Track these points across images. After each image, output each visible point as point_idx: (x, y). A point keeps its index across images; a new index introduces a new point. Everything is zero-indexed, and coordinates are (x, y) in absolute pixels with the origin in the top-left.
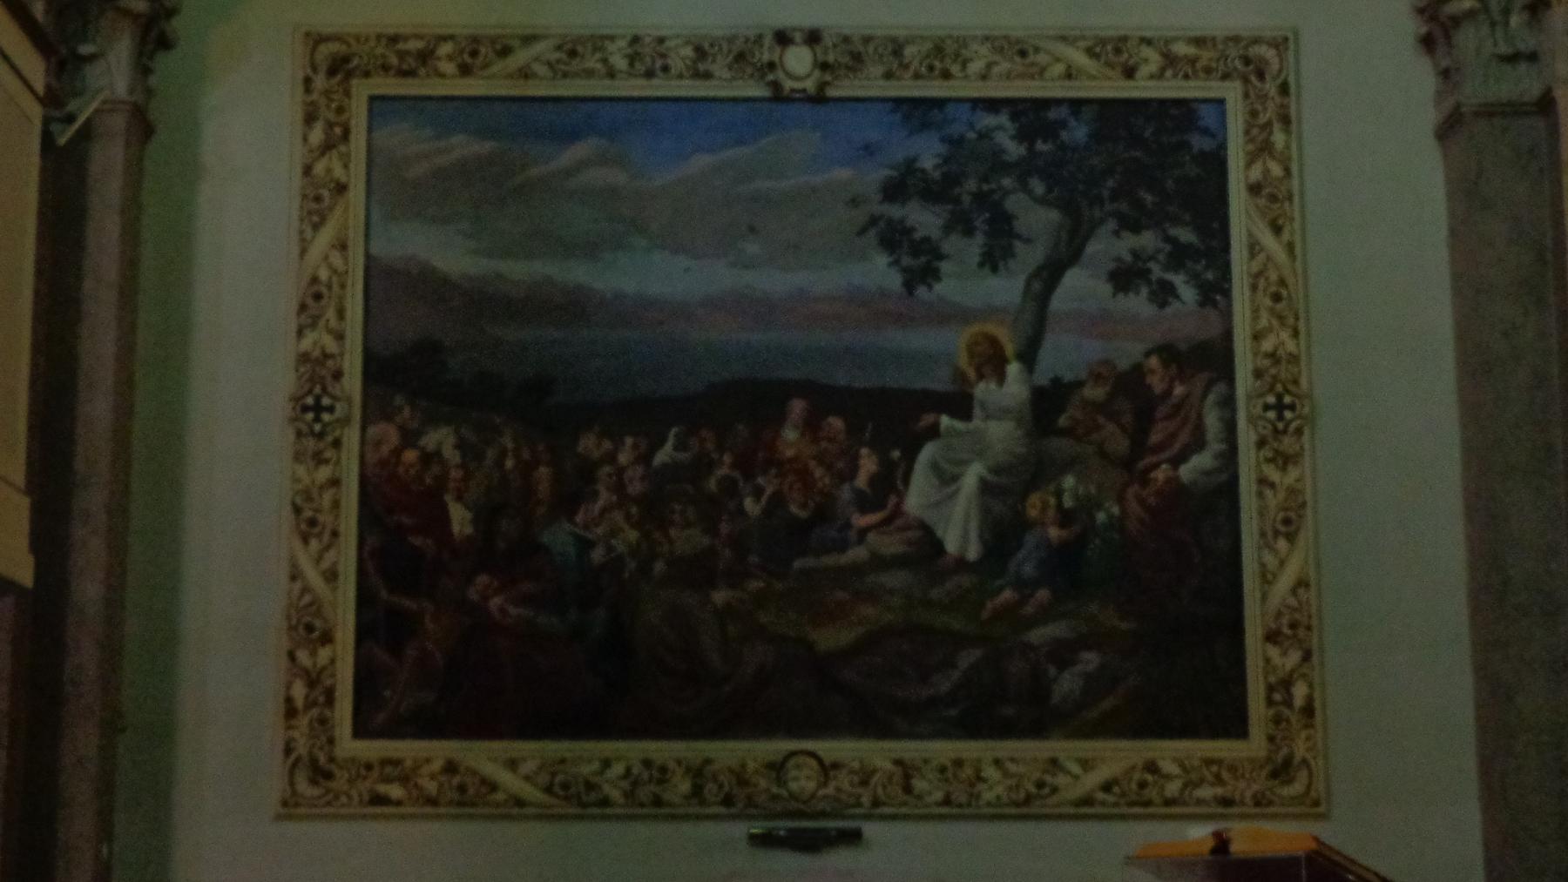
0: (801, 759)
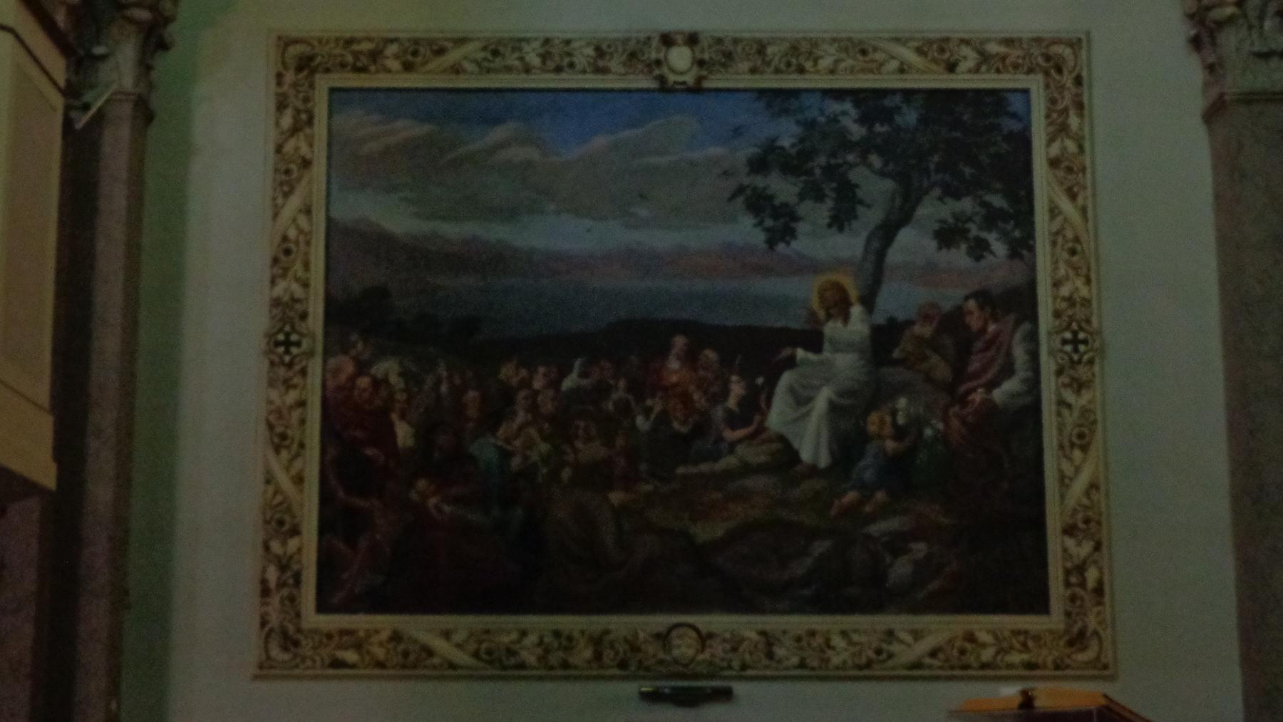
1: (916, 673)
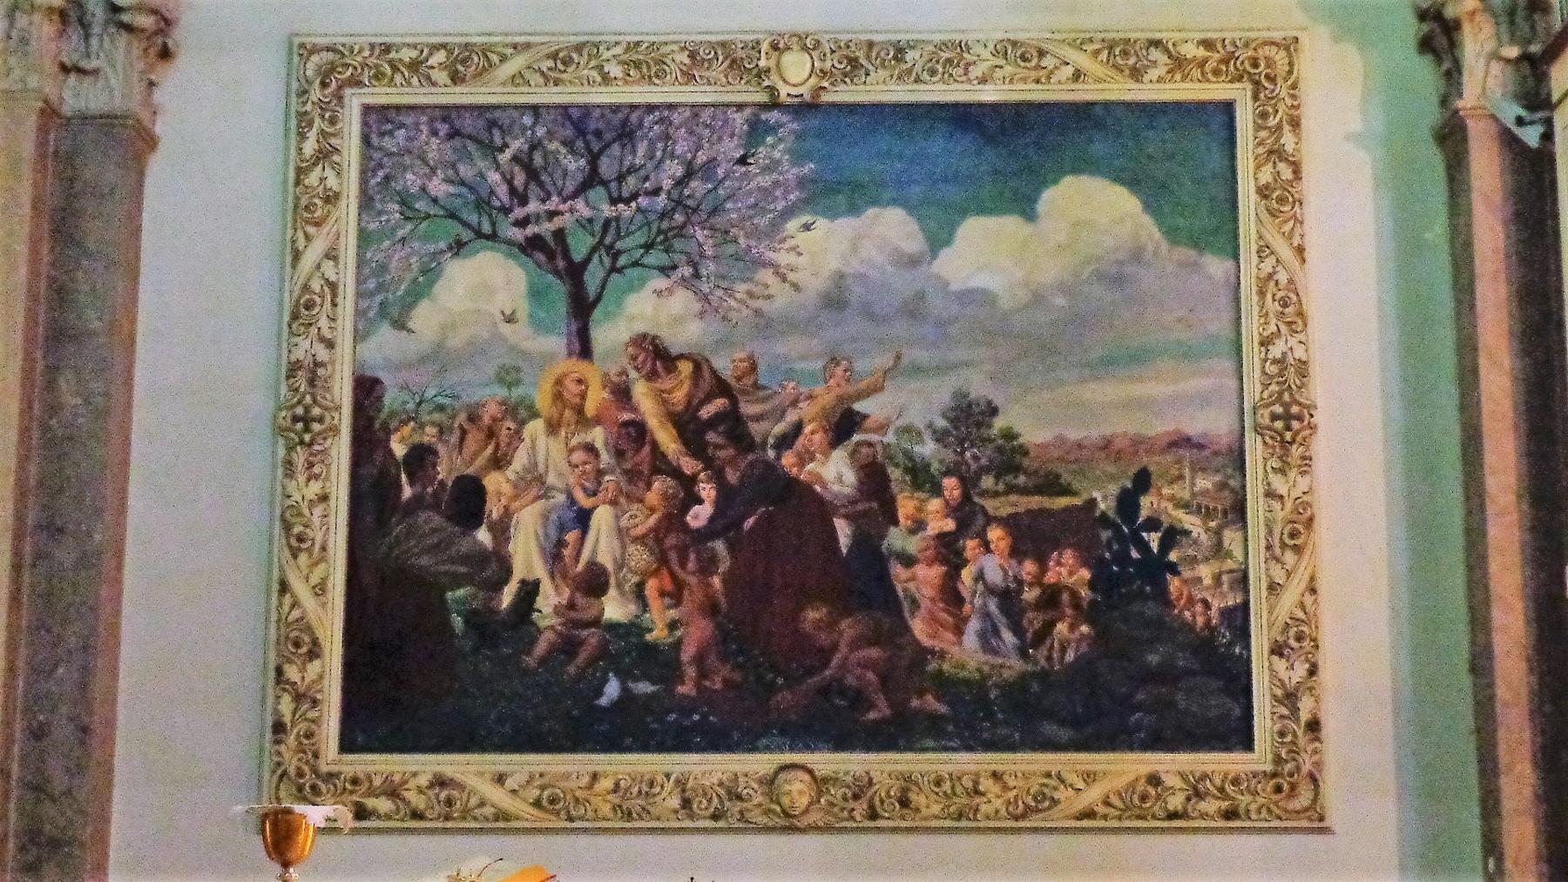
0: (791, 775)
1: (1086, 823)
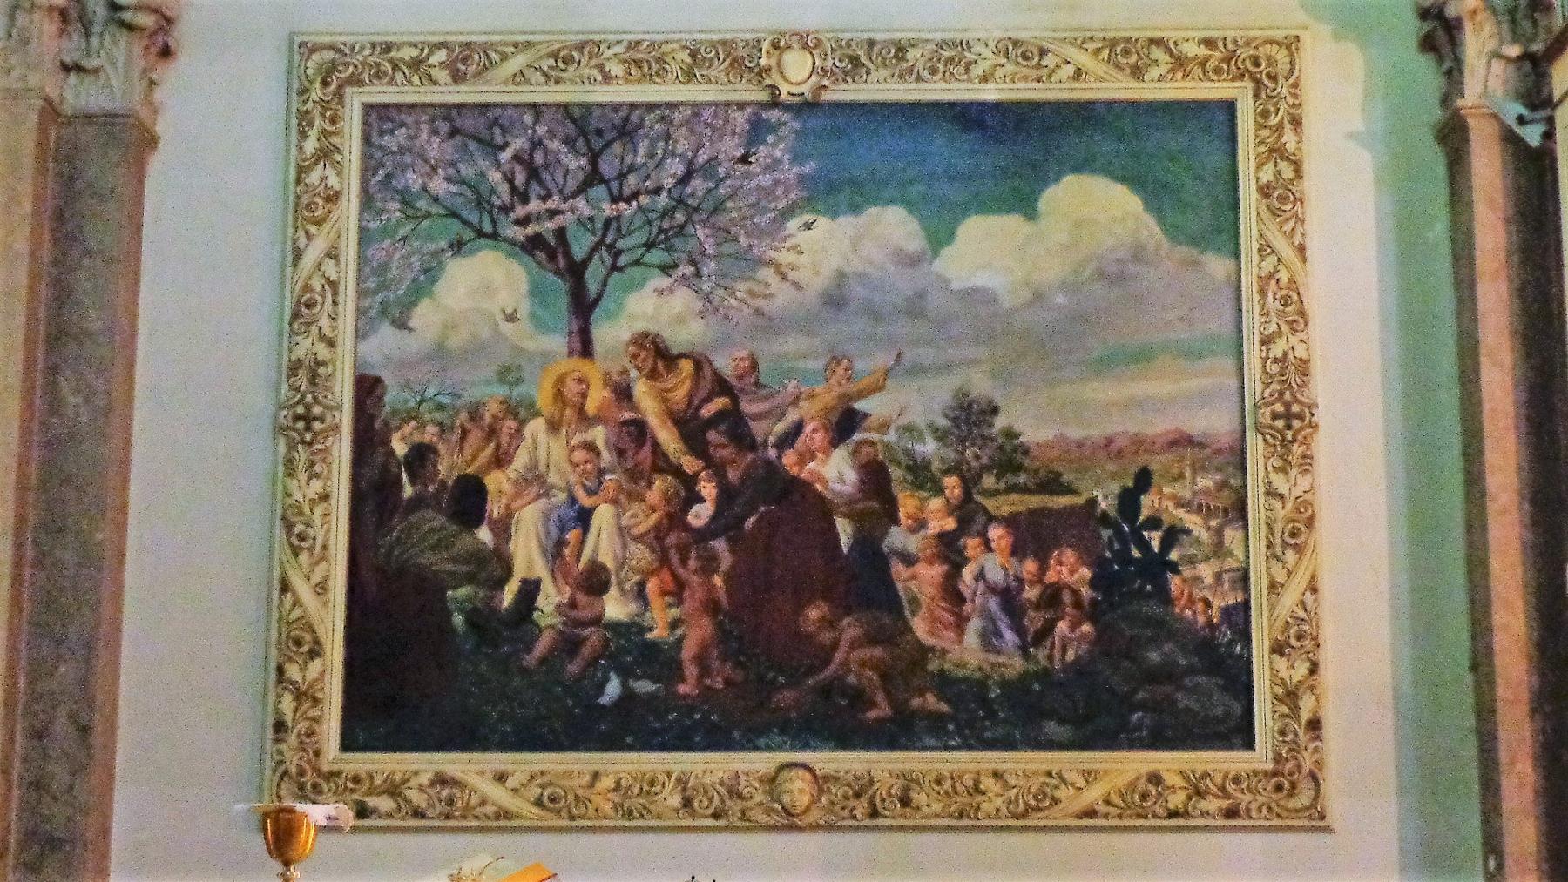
0: (793, 773)
